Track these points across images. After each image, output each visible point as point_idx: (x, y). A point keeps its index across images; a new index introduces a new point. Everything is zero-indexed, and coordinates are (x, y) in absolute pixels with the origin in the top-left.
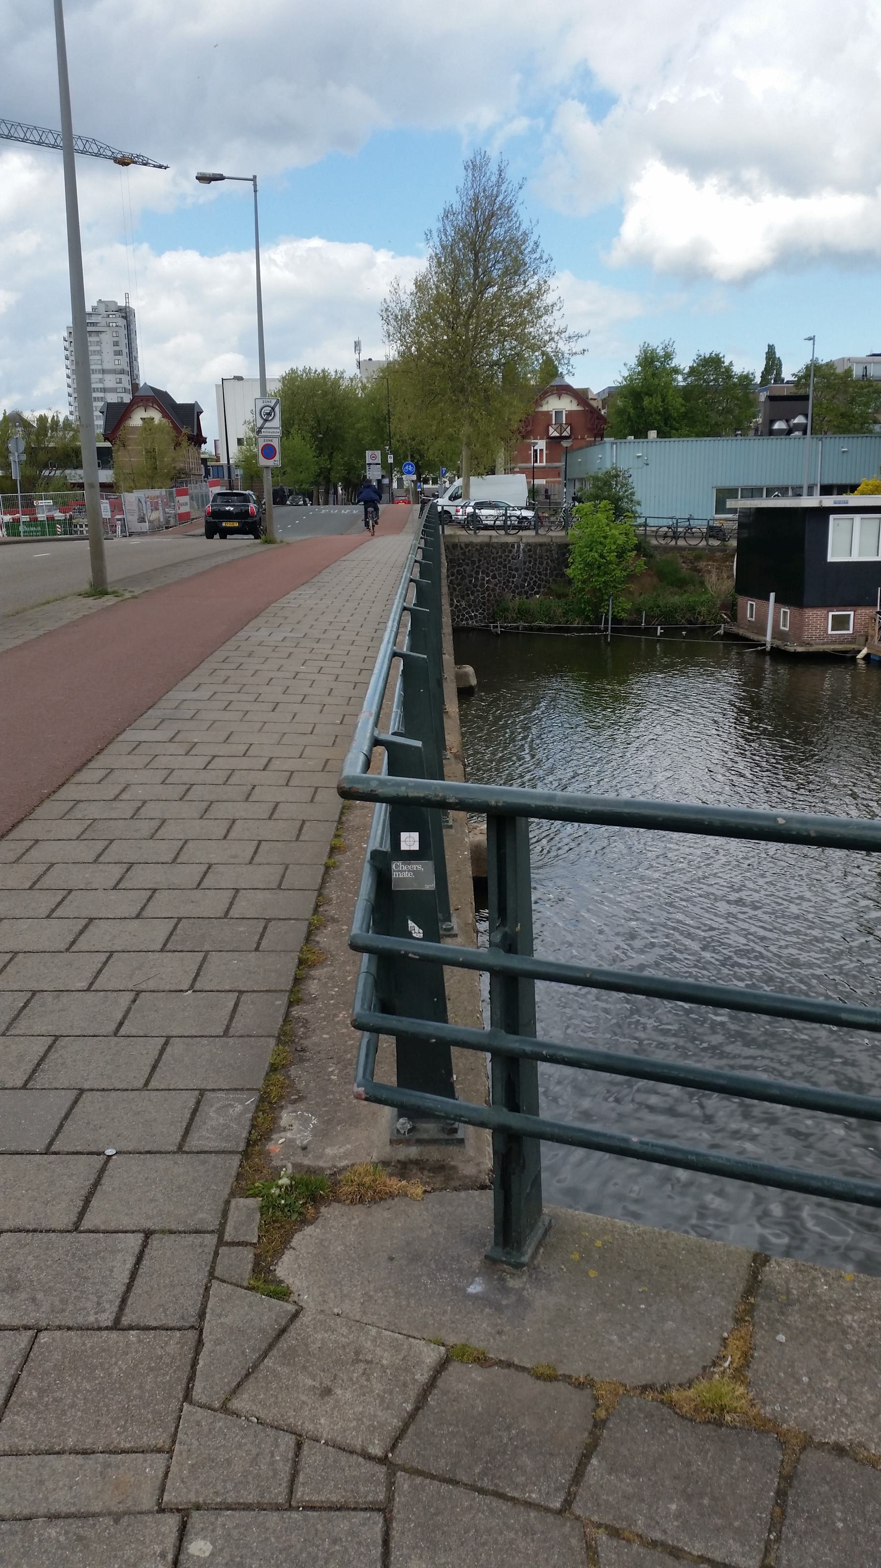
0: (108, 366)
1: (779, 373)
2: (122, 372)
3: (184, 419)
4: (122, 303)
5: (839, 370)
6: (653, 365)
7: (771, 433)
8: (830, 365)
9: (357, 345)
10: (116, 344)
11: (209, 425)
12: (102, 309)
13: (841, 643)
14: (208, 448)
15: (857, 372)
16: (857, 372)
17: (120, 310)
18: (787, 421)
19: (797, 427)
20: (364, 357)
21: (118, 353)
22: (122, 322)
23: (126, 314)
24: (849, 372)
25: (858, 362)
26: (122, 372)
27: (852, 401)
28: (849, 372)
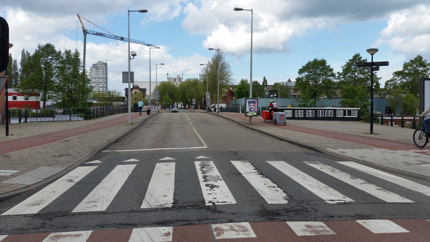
0: (100, 77)
1: (267, 83)
2: (104, 78)
3: (144, 91)
4: (105, 62)
5: (282, 85)
6: (276, 84)
7: (270, 97)
8: (280, 83)
9: (167, 74)
10: (103, 72)
11: (148, 93)
12: (100, 63)
13: (277, 219)
14: (146, 98)
15: (285, 85)
16: (285, 85)
17: (104, 63)
18: (403, 117)
19: (275, 96)
20: (169, 77)
21: (103, 74)
22: (105, 66)
23: (106, 64)
24: (283, 85)
25: (285, 83)
26: (104, 78)
27: (285, 91)
28: (283, 85)
